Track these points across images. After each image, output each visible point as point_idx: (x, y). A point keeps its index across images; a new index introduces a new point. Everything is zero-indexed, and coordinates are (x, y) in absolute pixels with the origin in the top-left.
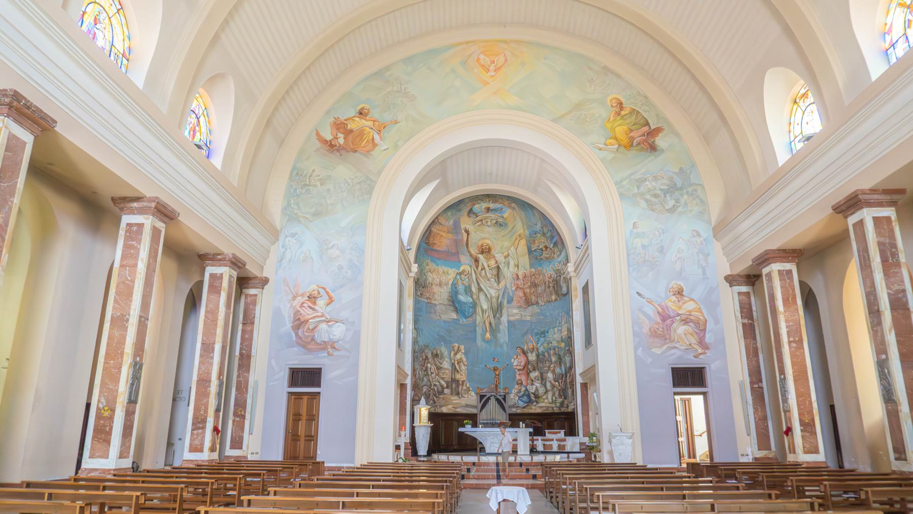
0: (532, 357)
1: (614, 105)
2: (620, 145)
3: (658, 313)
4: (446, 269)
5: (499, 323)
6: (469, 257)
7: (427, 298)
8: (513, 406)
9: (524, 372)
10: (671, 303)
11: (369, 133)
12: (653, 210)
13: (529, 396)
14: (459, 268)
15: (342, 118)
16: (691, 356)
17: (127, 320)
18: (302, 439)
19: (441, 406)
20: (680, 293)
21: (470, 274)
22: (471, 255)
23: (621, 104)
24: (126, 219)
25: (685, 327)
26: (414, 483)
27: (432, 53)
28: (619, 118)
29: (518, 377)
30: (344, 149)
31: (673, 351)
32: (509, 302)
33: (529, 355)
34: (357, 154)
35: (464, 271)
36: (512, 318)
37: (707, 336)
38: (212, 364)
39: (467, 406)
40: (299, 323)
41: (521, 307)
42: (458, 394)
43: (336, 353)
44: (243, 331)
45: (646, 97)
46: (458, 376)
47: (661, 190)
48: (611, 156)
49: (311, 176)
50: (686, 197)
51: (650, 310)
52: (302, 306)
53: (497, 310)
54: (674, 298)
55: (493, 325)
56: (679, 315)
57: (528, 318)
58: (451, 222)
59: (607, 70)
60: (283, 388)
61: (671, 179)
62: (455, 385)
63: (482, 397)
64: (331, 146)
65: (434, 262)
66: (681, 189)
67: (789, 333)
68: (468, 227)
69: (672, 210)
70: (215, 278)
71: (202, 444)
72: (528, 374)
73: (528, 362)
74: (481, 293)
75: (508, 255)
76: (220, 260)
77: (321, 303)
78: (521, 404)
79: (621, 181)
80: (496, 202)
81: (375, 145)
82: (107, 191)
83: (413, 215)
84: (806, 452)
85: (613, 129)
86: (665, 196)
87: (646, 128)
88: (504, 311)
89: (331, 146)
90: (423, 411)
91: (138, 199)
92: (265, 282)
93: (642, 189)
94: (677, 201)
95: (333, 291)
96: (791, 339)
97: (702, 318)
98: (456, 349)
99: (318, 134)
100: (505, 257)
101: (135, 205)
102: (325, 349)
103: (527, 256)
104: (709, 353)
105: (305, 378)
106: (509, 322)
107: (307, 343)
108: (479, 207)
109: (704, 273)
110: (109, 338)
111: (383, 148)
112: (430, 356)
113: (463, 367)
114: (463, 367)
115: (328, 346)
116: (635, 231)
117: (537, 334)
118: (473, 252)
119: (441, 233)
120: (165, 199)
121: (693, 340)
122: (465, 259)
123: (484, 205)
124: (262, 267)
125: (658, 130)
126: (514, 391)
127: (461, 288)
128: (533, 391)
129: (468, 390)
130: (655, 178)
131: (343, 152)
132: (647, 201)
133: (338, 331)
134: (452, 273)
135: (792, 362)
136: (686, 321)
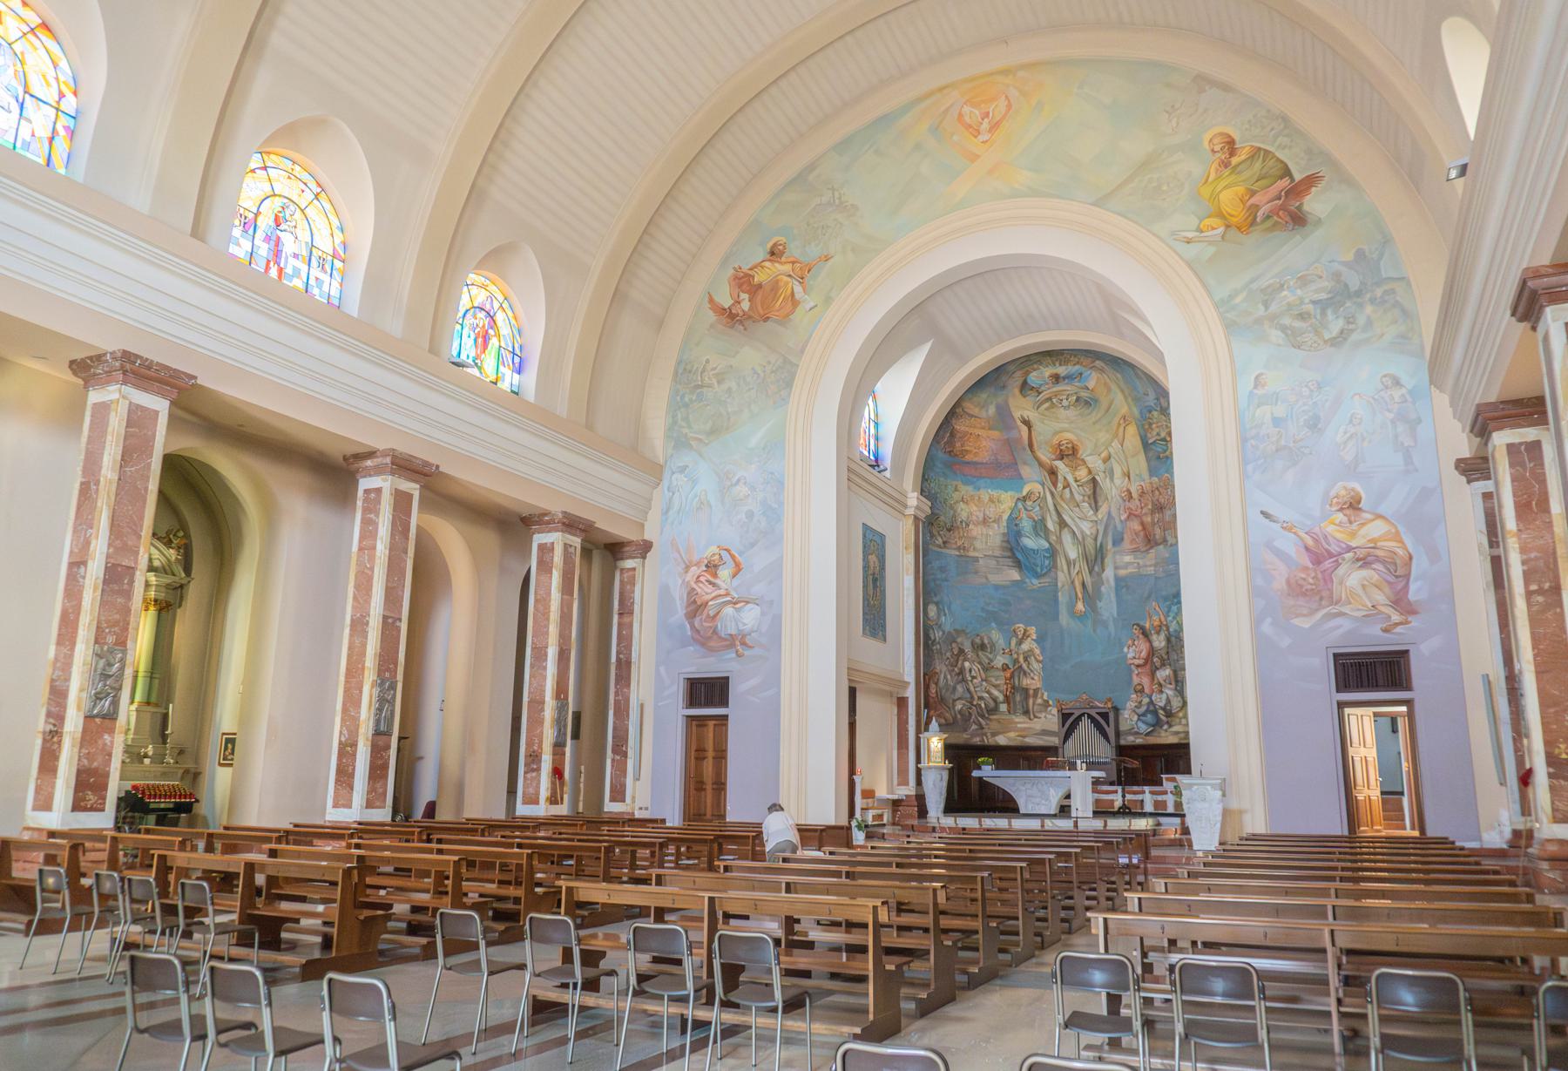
1: (1217, 148)
2: (1228, 226)
3: (1307, 549)
4: (995, 493)
5: (1098, 583)
7: (959, 548)
10: (1335, 528)
13: (1155, 713)
15: (745, 268)
17: (367, 624)
18: (709, 787)
19: (994, 735)
20: (1353, 505)
22: (1041, 464)
24: (365, 484)
25: (1364, 573)
26: (1364, 885)
27: (885, 120)
29: (1136, 680)
31: (1339, 621)
32: (1118, 541)
33: (1154, 637)
35: (1030, 493)
36: (1122, 572)
37: (1413, 587)
38: (545, 678)
40: (695, 608)
42: (1026, 712)
44: (620, 625)
46: (1026, 682)
47: (1314, 302)
48: (1212, 250)
50: (1369, 309)
51: (1289, 545)
52: (698, 581)
53: (1096, 559)
54: (1340, 517)
55: (1090, 588)
56: (1350, 549)
57: (1151, 570)
58: (992, 410)
59: (1202, 82)
60: (677, 711)
61: (1337, 276)
63: (1065, 717)
64: (731, 317)
67: (1527, 577)
70: (545, 550)
71: (538, 794)
72: (1153, 674)
73: (1152, 651)
76: (548, 523)
77: (724, 573)
78: (1143, 728)
79: (1231, 297)
80: (1066, 362)
81: (795, 303)
82: (336, 451)
83: (896, 406)
84: (1556, 820)
85: (1214, 197)
86: (1323, 313)
87: (1285, 182)
88: (1108, 561)
89: (731, 317)
91: (371, 454)
92: (646, 547)
93: (1274, 308)
94: (1350, 320)
95: (741, 553)
96: (1534, 587)
97: (1400, 552)
99: (711, 300)
100: (1105, 461)
101: (369, 463)
102: (733, 645)
104: (1415, 622)
105: (708, 692)
106: (1118, 579)
107: (707, 638)
108: (1040, 375)
109: (1408, 459)
110: (350, 648)
112: (968, 648)
113: (1035, 665)
114: (1035, 665)
115: (737, 642)
116: (1260, 392)
117: (1166, 599)
119: (977, 432)
120: (403, 448)
122: (1030, 472)
123: (1048, 371)
124: (643, 525)
125: (1311, 181)
126: (1131, 705)
127: (1026, 525)
129: (1046, 704)
130: (1303, 281)
131: (747, 323)
132: (1284, 329)
133: (750, 617)
134: (1007, 500)
135: (1533, 634)
136: (1364, 562)
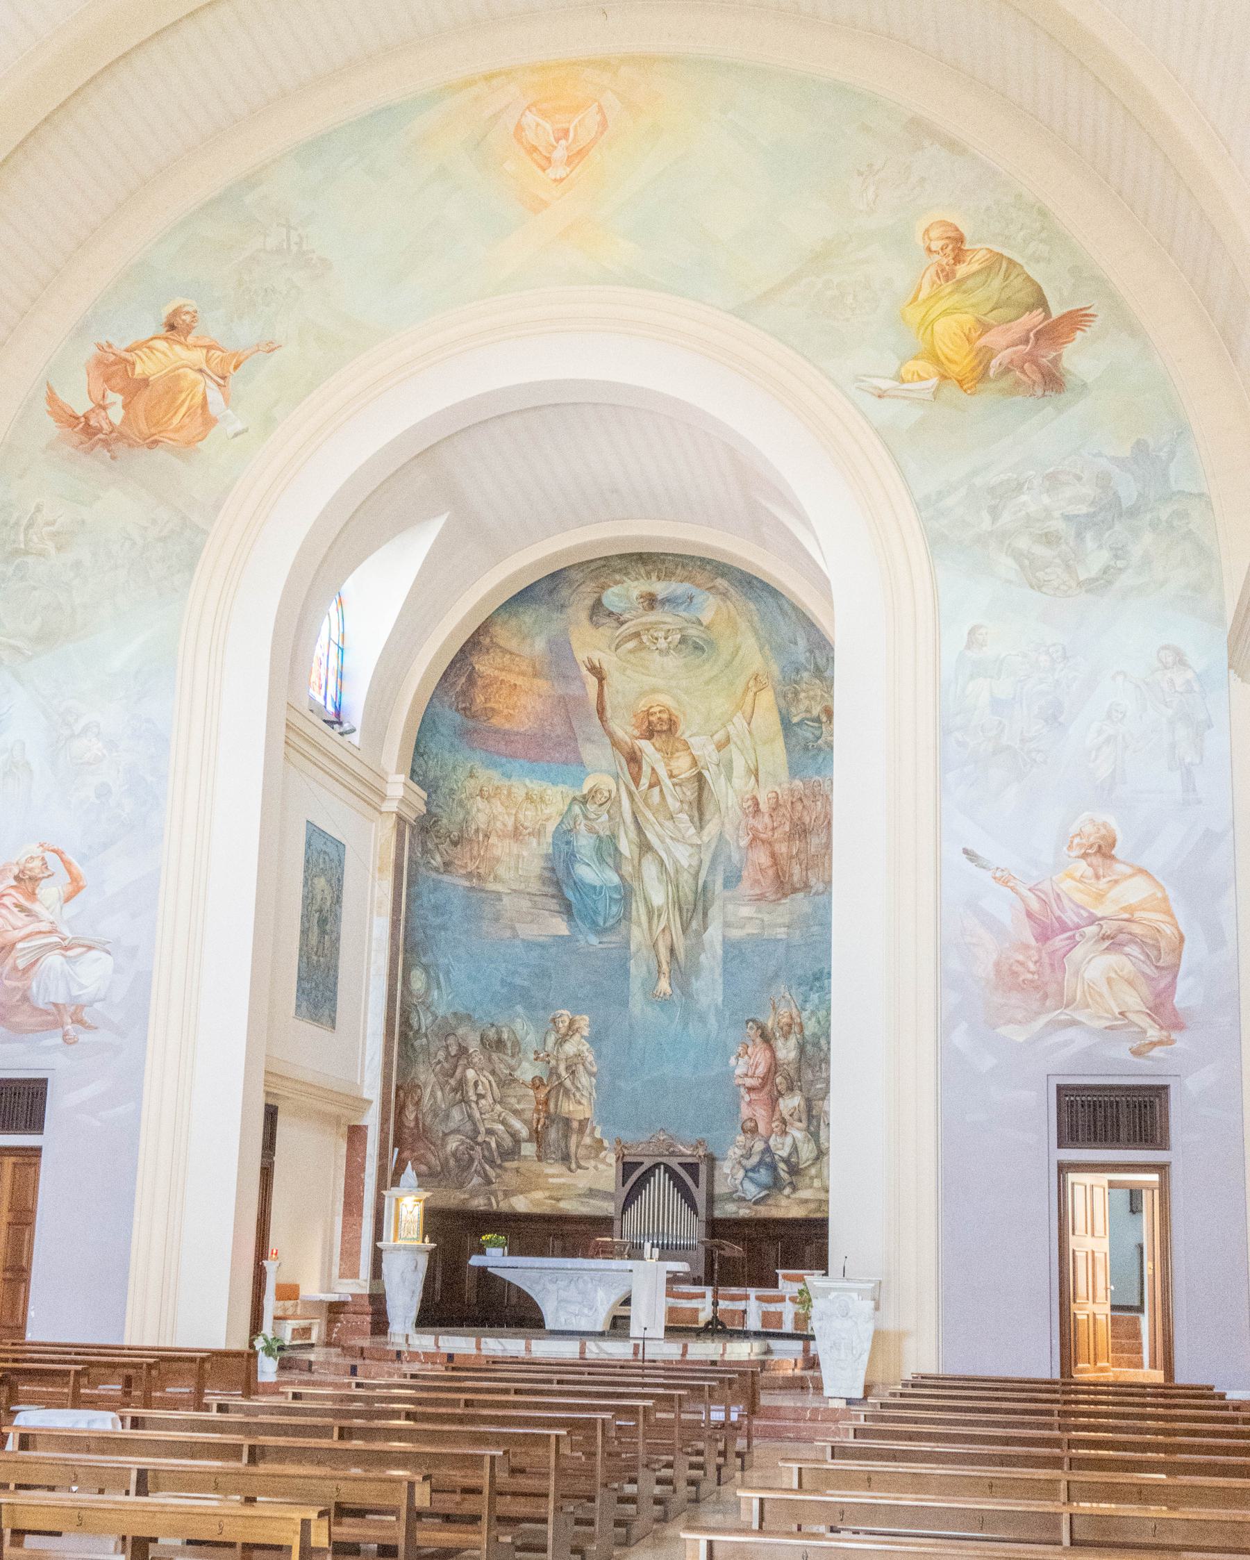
0: (787, 1051)
1: (936, 246)
2: (944, 377)
3: (1029, 915)
4: (535, 786)
5: (697, 947)
6: (609, 750)
7: (469, 876)
8: (730, 1198)
9: (763, 1095)
10: (1074, 886)
11: (195, 384)
12: (1038, 586)
13: (773, 1168)
14: (579, 782)
15: (120, 346)
16: (1121, 1052)
19: (507, 1194)
20: (1103, 850)
21: (612, 801)
22: (615, 743)
23: (960, 239)
25: (1113, 959)
28: (948, 287)
29: (745, 1112)
30: (122, 437)
31: (1071, 1033)
32: (732, 880)
33: (779, 1043)
34: (159, 454)
35: (594, 792)
36: (736, 934)
37: (1182, 985)
39: (592, 1193)
41: (761, 898)
42: (566, 1158)
43: (85, 1037)
45: (1043, 213)
47: (1067, 518)
49: (30, 525)
50: (1148, 538)
51: (1004, 908)
53: (694, 907)
54: (1082, 867)
56: (1093, 920)
57: (781, 933)
58: (540, 645)
61: (1103, 481)
62: (553, 1134)
63: (627, 1168)
64: (86, 431)
65: (495, 765)
66: (1133, 512)
68: (597, 657)
69: (1101, 583)
73: (774, 1067)
74: (649, 856)
75: (728, 740)
77: (50, 892)
78: (752, 1191)
80: (669, 575)
81: (209, 422)
86: (1079, 536)
88: (714, 912)
89: (86, 431)
90: (409, 1206)
93: (1006, 517)
94: (1119, 552)
97: (1168, 930)
98: (563, 1027)
99: (52, 398)
100: (720, 747)
102: (58, 1024)
103: (780, 744)
104: (1181, 1041)
106: (728, 944)
108: (623, 593)
111: (231, 430)
112: (474, 1045)
113: (584, 1080)
115: (65, 1018)
118: (620, 733)
119: (512, 679)
121: (1133, 1000)
125: (1076, 320)
126: (734, 1152)
127: (584, 843)
128: (784, 1153)
130: (1053, 481)
131: (120, 449)
132: (1018, 556)
133: (91, 976)
134: (556, 798)
136: (1113, 941)
